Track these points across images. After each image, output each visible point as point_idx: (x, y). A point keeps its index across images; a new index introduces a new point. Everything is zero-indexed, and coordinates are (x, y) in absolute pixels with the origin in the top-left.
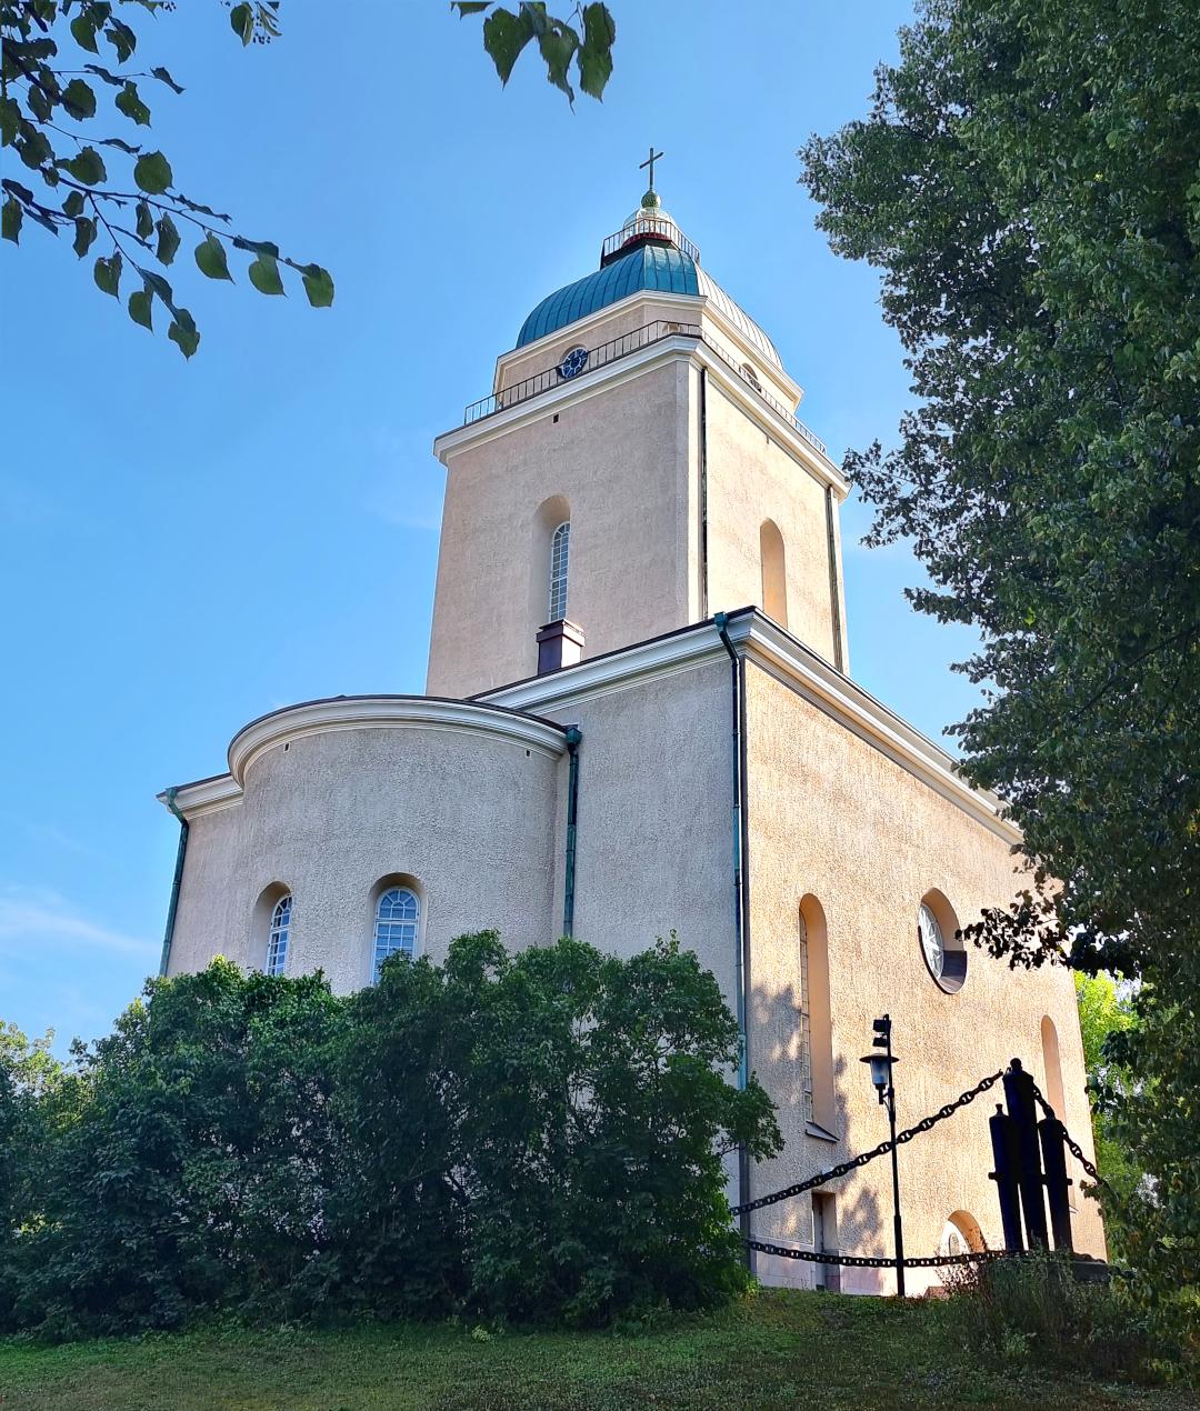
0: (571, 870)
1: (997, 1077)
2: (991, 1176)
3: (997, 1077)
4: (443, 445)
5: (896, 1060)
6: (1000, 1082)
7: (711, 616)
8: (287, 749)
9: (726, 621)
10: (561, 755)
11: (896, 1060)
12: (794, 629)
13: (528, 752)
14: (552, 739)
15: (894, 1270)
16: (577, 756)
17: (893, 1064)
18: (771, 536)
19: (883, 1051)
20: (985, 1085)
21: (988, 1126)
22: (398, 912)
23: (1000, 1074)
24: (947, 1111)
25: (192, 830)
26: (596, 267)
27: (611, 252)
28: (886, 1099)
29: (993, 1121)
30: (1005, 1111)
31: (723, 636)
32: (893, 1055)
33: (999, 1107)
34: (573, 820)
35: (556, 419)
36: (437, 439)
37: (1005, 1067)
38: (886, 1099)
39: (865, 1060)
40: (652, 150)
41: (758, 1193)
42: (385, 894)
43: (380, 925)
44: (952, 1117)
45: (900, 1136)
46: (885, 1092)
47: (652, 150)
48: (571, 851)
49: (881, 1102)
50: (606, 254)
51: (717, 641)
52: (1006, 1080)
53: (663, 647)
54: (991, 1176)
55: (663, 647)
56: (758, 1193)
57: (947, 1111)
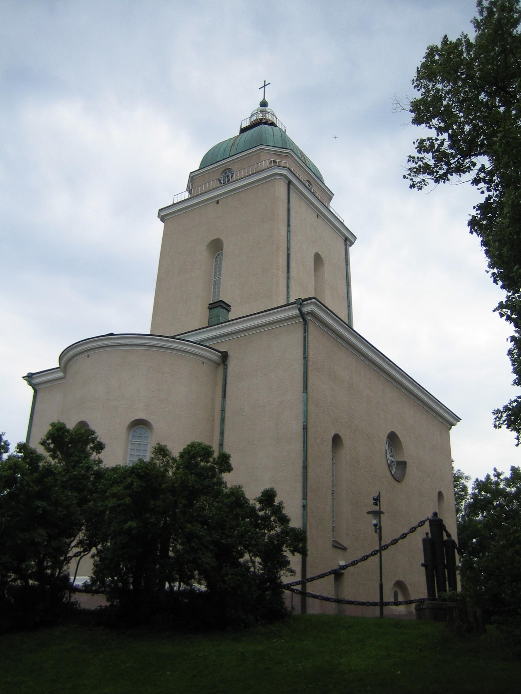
0: (223, 420)
1: (426, 520)
2: (423, 565)
3: (426, 520)
4: (163, 214)
5: (383, 513)
6: (427, 523)
7: (292, 300)
8: (88, 357)
9: (300, 303)
10: (219, 364)
11: (383, 513)
12: (328, 303)
13: (203, 363)
14: (215, 357)
15: (385, 600)
16: (227, 365)
17: (381, 515)
18: (318, 259)
19: (377, 508)
20: (422, 524)
21: (422, 543)
22: (140, 437)
23: (428, 519)
24: (404, 536)
25: (38, 393)
26: (237, 133)
27: (245, 126)
28: (378, 530)
29: (424, 540)
30: (430, 536)
31: (300, 310)
32: (381, 510)
33: (427, 534)
34: (224, 396)
35: (218, 202)
36: (160, 210)
37: (430, 515)
38: (378, 530)
39: (369, 513)
40: (265, 81)
41: (309, 576)
42: (133, 429)
43: (132, 444)
44: (366, 561)
45: (377, 553)
46: (377, 527)
47: (265, 81)
48: (223, 411)
49: (376, 532)
50: (242, 127)
51: (296, 312)
52: (431, 522)
53: (268, 314)
54: (423, 565)
55: (268, 314)
56: (309, 576)
57: (404, 536)
